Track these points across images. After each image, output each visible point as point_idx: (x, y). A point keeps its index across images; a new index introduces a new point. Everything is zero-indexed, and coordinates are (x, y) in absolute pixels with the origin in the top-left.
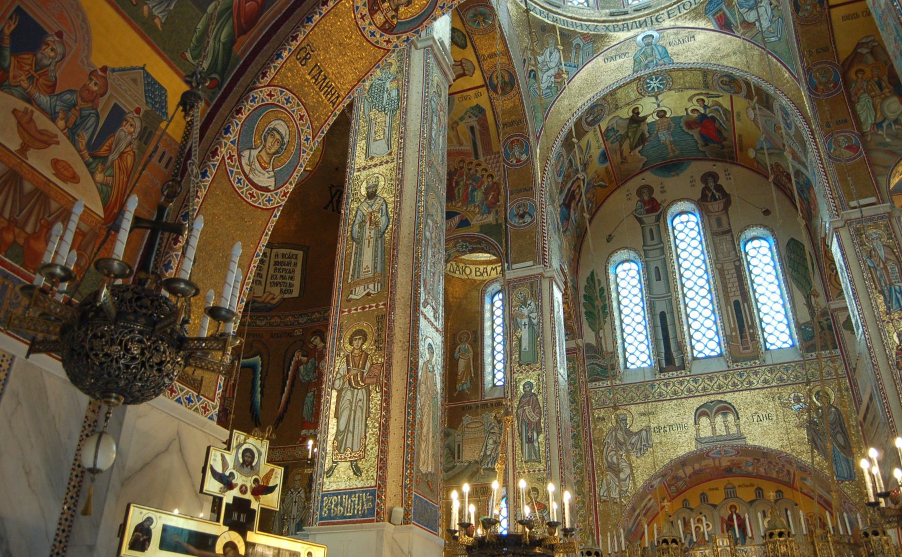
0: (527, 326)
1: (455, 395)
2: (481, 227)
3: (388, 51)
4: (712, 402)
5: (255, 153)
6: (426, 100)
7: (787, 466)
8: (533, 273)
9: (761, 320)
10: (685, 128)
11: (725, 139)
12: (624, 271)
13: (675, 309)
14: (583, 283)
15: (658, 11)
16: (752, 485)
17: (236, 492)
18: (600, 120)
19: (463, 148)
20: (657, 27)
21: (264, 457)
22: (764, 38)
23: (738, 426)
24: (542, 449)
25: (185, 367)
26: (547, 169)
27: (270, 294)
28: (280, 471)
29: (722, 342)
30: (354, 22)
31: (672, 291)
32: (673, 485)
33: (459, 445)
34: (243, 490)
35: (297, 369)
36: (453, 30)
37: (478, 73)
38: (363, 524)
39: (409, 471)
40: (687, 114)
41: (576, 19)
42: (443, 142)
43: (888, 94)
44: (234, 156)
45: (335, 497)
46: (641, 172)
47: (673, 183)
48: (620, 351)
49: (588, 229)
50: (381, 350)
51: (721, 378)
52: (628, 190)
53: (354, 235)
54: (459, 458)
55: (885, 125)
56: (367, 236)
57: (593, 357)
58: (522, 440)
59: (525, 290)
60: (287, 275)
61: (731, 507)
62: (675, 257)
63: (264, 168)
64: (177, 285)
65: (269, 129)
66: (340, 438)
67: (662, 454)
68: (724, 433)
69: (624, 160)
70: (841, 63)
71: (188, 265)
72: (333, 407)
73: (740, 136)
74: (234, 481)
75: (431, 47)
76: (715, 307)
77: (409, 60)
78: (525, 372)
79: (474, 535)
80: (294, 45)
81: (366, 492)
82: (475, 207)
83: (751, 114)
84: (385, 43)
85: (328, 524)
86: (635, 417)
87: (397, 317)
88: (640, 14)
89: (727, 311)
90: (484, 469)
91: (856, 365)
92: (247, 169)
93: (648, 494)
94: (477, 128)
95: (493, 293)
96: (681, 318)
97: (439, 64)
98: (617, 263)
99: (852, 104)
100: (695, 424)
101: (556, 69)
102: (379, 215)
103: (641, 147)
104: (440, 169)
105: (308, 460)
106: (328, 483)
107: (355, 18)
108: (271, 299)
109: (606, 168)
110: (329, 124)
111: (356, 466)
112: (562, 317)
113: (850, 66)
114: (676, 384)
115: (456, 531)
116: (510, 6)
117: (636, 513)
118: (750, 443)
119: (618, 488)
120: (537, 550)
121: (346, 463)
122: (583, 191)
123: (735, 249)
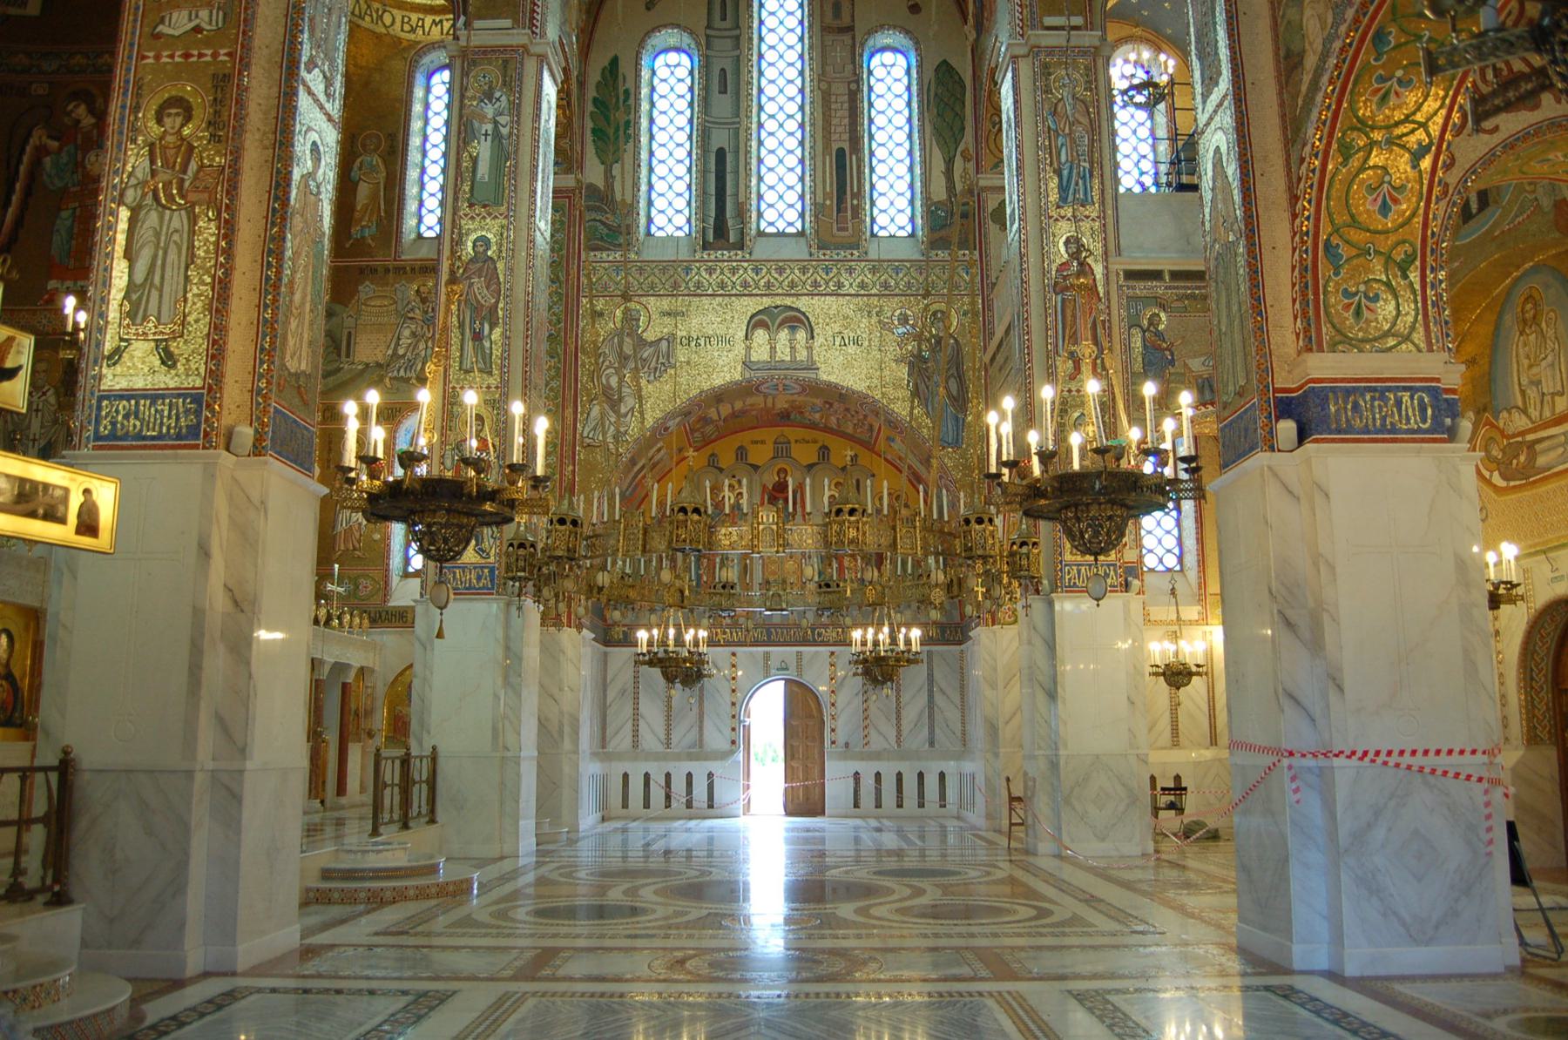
0: (489, 138)
1: (347, 246)
4: (776, 307)
7: (871, 418)
8: (510, 43)
9: (872, 187)
13: (742, 146)
14: (594, 77)
16: (815, 442)
23: (810, 349)
24: (497, 352)
31: (742, 114)
32: (698, 430)
35: (37, 163)
38: (179, 451)
39: (265, 366)
48: (643, 204)
50: (219, 141)
51: (796, 271)
54: (348, 356)
62: (755, 58)
66: (134, 297)
68: (788, 358)
72: (121, 238)
76: (807, 154)
78: (478, 219)
81: (185, 396)
86: (654, 317)
89: (824, 164)
93: (657, 441)
96: (750, 164)
98: (657, 49)
100: (746, 338)
105: (66, 334)
106: (111, 377)
111: (166, 350)
112: (553, 130)
114: (726, 271)
115: (351, 469)
117: (636, 468)
118: (824, 377)
121: (146, 344)
123: (854, 62)
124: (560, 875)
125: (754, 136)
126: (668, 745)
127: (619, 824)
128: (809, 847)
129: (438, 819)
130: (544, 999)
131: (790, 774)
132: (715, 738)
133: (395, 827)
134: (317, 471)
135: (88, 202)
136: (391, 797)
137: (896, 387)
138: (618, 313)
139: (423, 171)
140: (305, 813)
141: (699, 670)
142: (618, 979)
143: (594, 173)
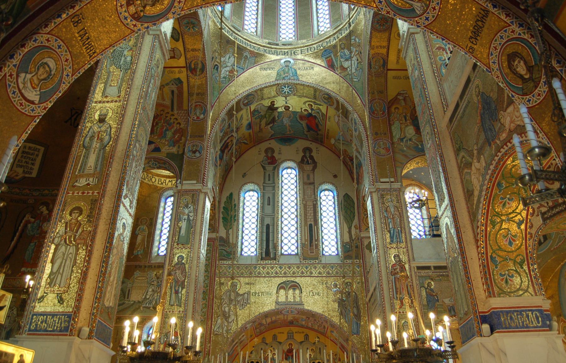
0: (186, 221)
1: (132, 257)
2: (168, 154)
3: (134, 31)
4: (288, 281)
5: (29, 76)
6: (149, 68)
7: (324, 324)
9: (322, 237)
10: (298, 119)
11: (320, 130)
12: (250, 196)
14: (224, 199)
15: (296, 48)
16: (303, 333)
18: (251, 104)
19: (164, 102)
20: (294, 57)
23: (301, 297)
24: (183, 298)
26: (214, 126)
27: (15, 172)
28: (9, 296)
29: (299, 247)
30: (115, 7)
31: (276, 213)
35: (25, 226)
36: (174, 29)
37: (183, 58)
39: (97, 304)
40: (301, 111)
41: (248, 41)
42: (155, 97)
43: (409, 124)
44: (13, 75)
45: (42, 317)
46: (269, 140)
47: (286, 149)
48: (239, 244)
50: (91, 222)
51: (295, 268)
52: (260, 149)
53: (85, 144)
54: (128, 298)
55: (404, 140)
56: (94, 146)
57: (223, 245)
58: (171, 291)
59: (189, 198)
60: (30, 161)
61: (289, 344)
62: (280, 193)
63: (34, 88)
65: (42, 63)
66: (52, 277)
67: (255, 309)
68: (293, 301)
69: (261, 130)
70: (388, 101)
72: (51, 255)
75: (158, 35)
76: (299, 226)
77: (142, 40)
78: (180, 249)
80: (71, 12)
81: (65, 315)
82: (166, 141)
84: (133, 26)
86: (242, 285)
87: (105, 202)
88: (286, 47)
90: (143, 307)
91: (369, 270)
92: (21, 86)
95: (167, 197)
97: (161, 47)
98: (246, 191)
99: (390, 125)
100: (277, 293)
101: (231, 68)
102: (105, 135)
103: (271, 125)
104: (150, 113)
105: (25, 289)
106: (38, 307)
108: (15, 176)
109: (250, 134)
110: (84, 69)
111: (61, 297)
112: (208, 218)
113: (393, 104)
116: (210, 23)
118: (306, 308)
125: (280, 220)
134: (112, 345)
137: (334, 311)
138: (229, 283)
143: (222, 233)
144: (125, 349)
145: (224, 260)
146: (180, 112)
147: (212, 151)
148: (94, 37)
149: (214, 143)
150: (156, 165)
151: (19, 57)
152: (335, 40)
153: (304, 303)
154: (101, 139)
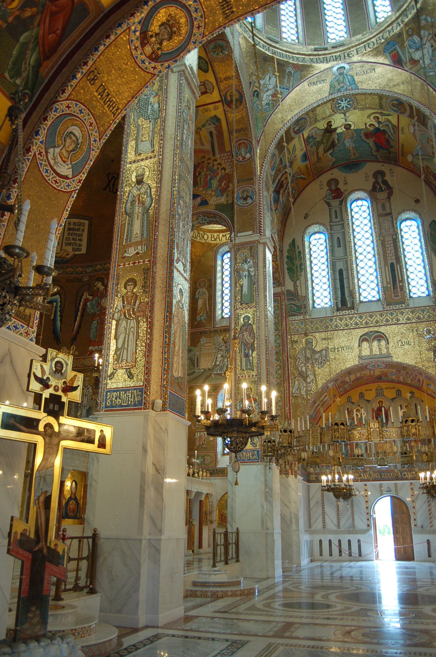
3: (155, 75)
4: (371, 332)
5: (57, 150)
6: (179, 112)
7: (419, 376)
8: (252, 240)
9: (408, 277)
10: (363, 138)
14: (286, 248)
15: (349, 48)
16: (394, 388)
17: (51, 390)
18: (303, 130)
19: (204, 147)
20: (348, 61)
21: (70, 367)
22: (425, 73)
23: (387, 348)
24: (255, 361)
25: (19, 307)
27: (66, 251)
28: (81, 376)
29: (381, 291)
30: (129, 52)
31: (348, 254)
32: (342, 387)
33: (198, 358)
34: (56, 389)
35: (85, 304)
36: (200, 58)
37: (216, 91)
40: (366, 127)
45: (115, 393)
47: (353, 178)
48: (310, 295)
49: (292, 209)
50: (147, 293)
51: (378, 316)
52: (321, 182)
53: (127, 211)
54: (197, 366)
56: (136, 212)
57: (292, 299)
59: (246, 252)
60: (78, 238)
62: (351, 231)
63: (64, 162)
64: (14, 250)
65: (67, 133)
66: (118, 353)
68: (378, 353)
69: (319, 159)
71: (21, 236)
72: (113, 332)
73: (403, 145)
74: (50, 383)
75: (183, 71)
76: (377, 267)
77: (167, 81)
79: (211, 419)
80: (85, 69)
82: (212, 191)
83: (412, 128)
84: (152, 69)
85: (111, 410)
87: (158, 269)
88: (337, 50)
89: (385, 271)
92: (52, 162)
93: (325, 392)
94: (215, 132)
96: (353, 274)
97: (189, 84)
98: (311, 234)
100: (359, 346)
101: (273, 90)
102: (145, 197)
103: (331, 151)
104: (189, 163)
105: (95, 367)
107: (130, 49)
109: (306, 165)
110: (111, 130)
111: (130, 372)
112: (271, 271)
116: (241, 41)
117: (316, 405)
118: (395, 360)
119: (305, 389)
120: (253, 429)
121: (123, 370)
122: (290, 180)
124: (293, 587)
125: (354, 263)
126: (339, 527)
127: (319, 564)
128: (409, 577)
129: (240, 560)
130: (287, 648)
131: (396, 541)
132: (360, 524)
133: (223, 563)
134: (187, 415)
135: (102, 317)
136: (220, 550)
137: (429, 361)
138: (304, 340)
139: (223, 292)
140: (186, 556)
141: (350, 493)
142: (320, 640)
143: (289, 285)
144: (200, 418)
145: (294, 315)
146: (222, 155)
147: (265, 195)
148: (114, 91)
149: (266, 185)
150: (205, 220)
151: (44, 132)
152: (400, 25)
153: (392, 355)
154: (142, 203)
